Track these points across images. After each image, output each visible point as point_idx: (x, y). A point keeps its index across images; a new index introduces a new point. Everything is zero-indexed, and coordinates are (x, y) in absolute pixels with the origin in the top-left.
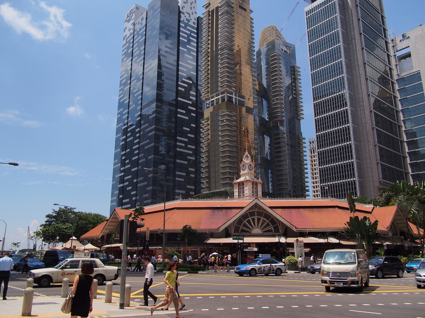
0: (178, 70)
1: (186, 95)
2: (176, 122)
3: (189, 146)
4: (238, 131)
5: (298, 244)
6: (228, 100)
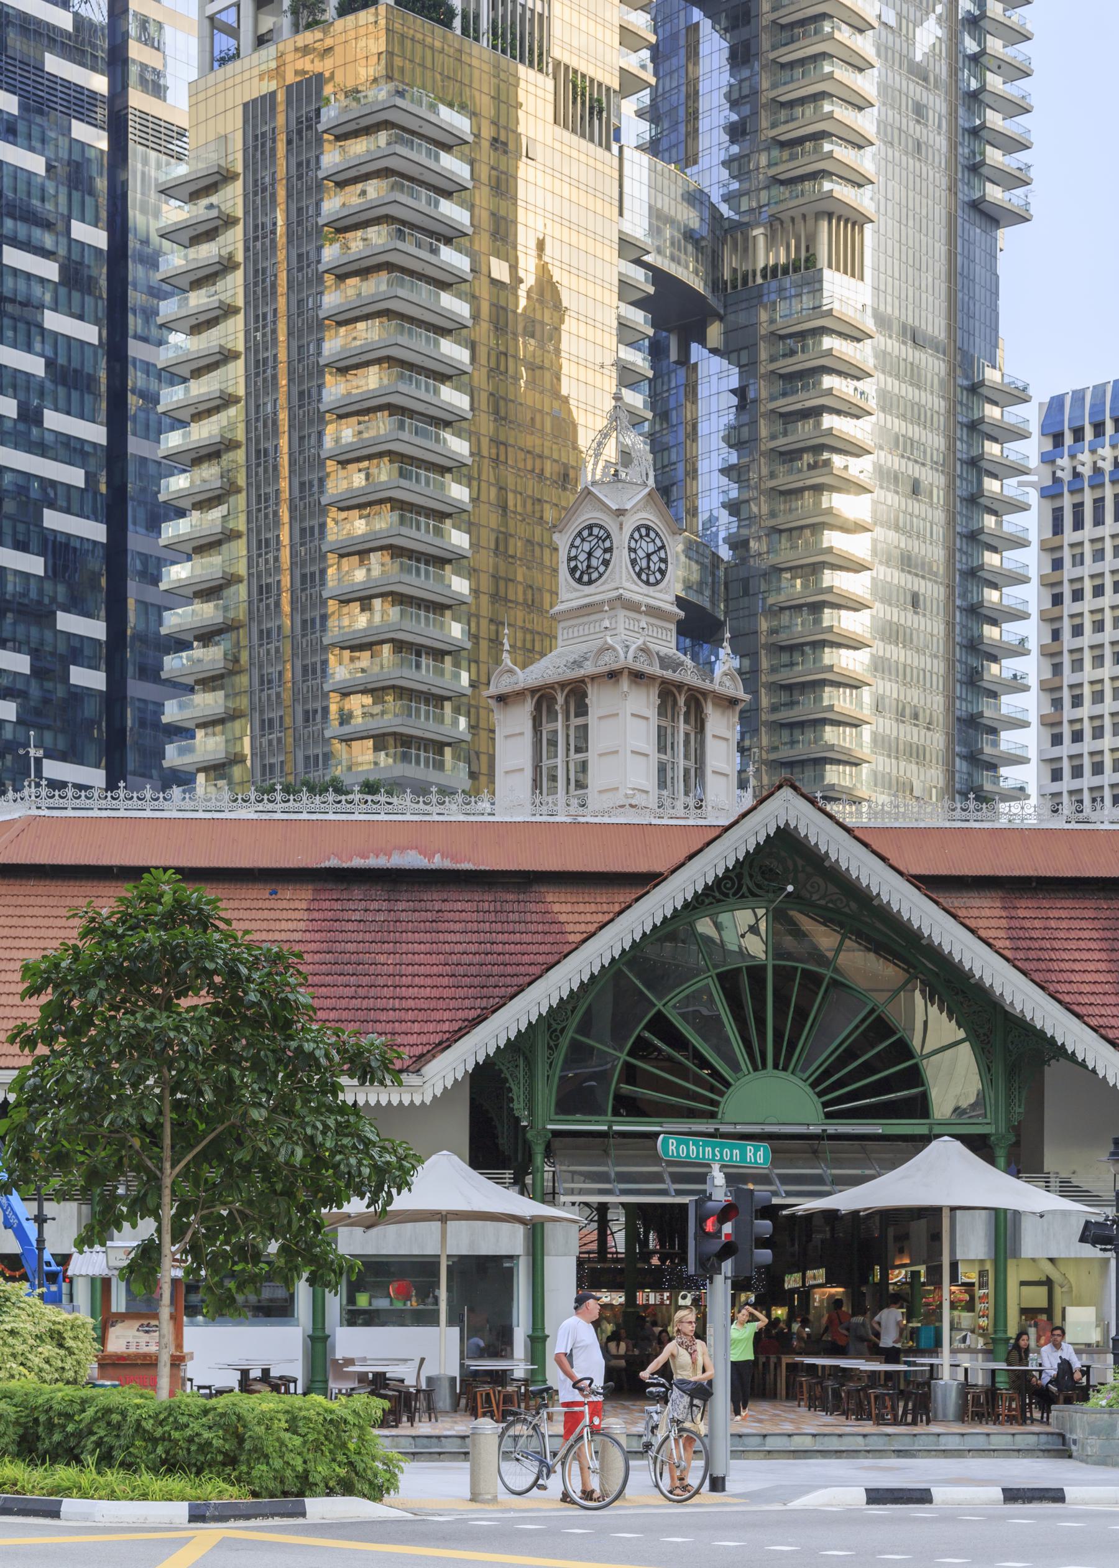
3: (54, 420)
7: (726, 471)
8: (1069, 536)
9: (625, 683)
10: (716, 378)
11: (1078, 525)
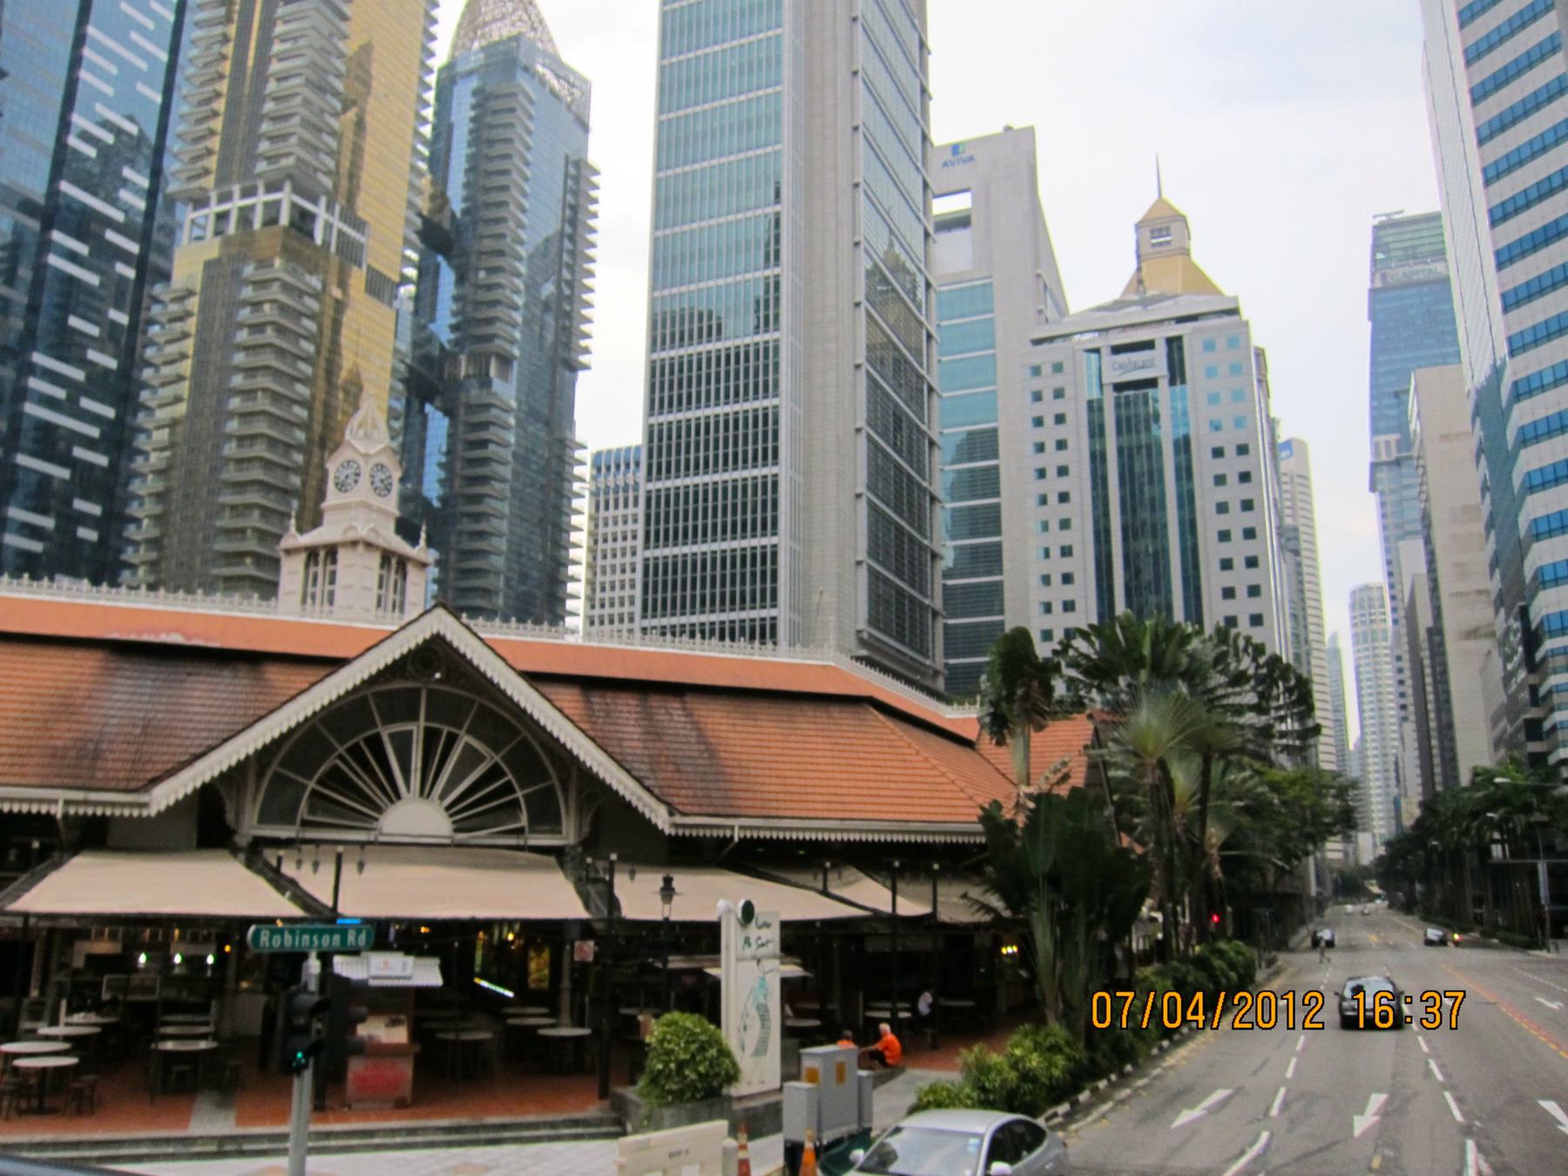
0: (76, 62)
1: (103, 180)
2: (37, 286)
3: (86, 403)
4: (322, 363)
5: (747, 941)
6: (292, 224)
7: (440, 465)
8: (602, 513)
9: (361, 548)
10: (438, 425)
11: (607, 508)
